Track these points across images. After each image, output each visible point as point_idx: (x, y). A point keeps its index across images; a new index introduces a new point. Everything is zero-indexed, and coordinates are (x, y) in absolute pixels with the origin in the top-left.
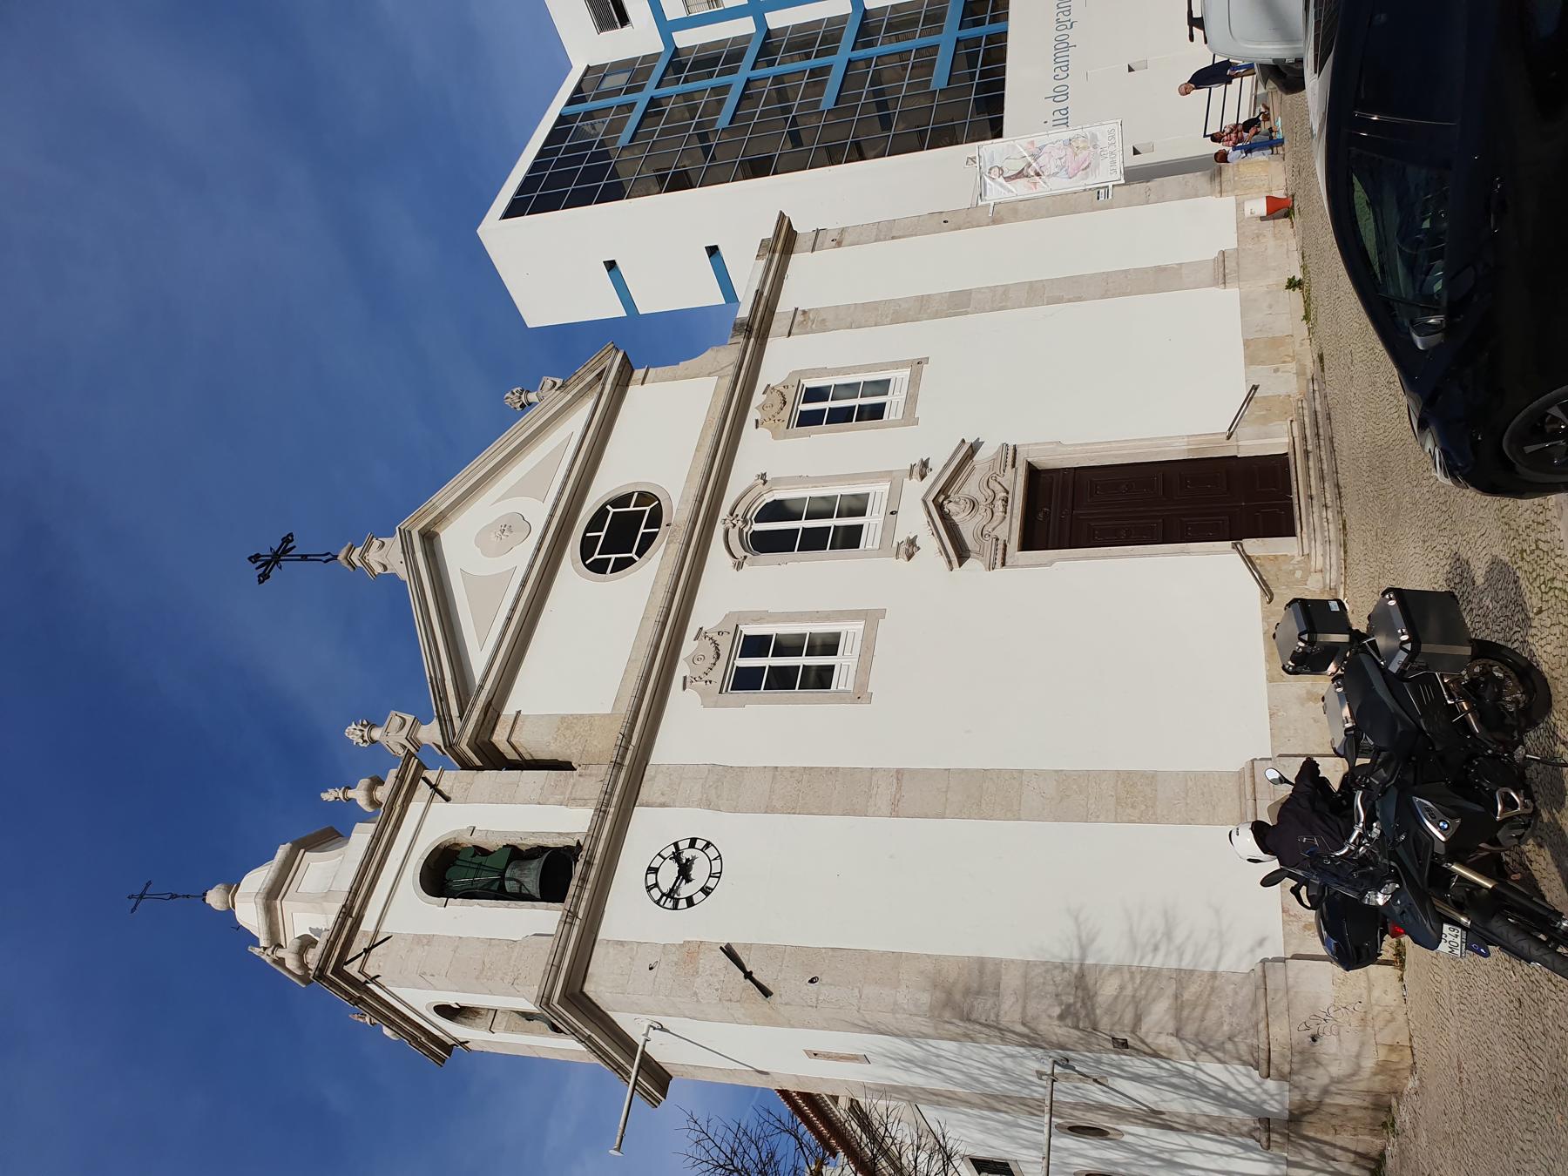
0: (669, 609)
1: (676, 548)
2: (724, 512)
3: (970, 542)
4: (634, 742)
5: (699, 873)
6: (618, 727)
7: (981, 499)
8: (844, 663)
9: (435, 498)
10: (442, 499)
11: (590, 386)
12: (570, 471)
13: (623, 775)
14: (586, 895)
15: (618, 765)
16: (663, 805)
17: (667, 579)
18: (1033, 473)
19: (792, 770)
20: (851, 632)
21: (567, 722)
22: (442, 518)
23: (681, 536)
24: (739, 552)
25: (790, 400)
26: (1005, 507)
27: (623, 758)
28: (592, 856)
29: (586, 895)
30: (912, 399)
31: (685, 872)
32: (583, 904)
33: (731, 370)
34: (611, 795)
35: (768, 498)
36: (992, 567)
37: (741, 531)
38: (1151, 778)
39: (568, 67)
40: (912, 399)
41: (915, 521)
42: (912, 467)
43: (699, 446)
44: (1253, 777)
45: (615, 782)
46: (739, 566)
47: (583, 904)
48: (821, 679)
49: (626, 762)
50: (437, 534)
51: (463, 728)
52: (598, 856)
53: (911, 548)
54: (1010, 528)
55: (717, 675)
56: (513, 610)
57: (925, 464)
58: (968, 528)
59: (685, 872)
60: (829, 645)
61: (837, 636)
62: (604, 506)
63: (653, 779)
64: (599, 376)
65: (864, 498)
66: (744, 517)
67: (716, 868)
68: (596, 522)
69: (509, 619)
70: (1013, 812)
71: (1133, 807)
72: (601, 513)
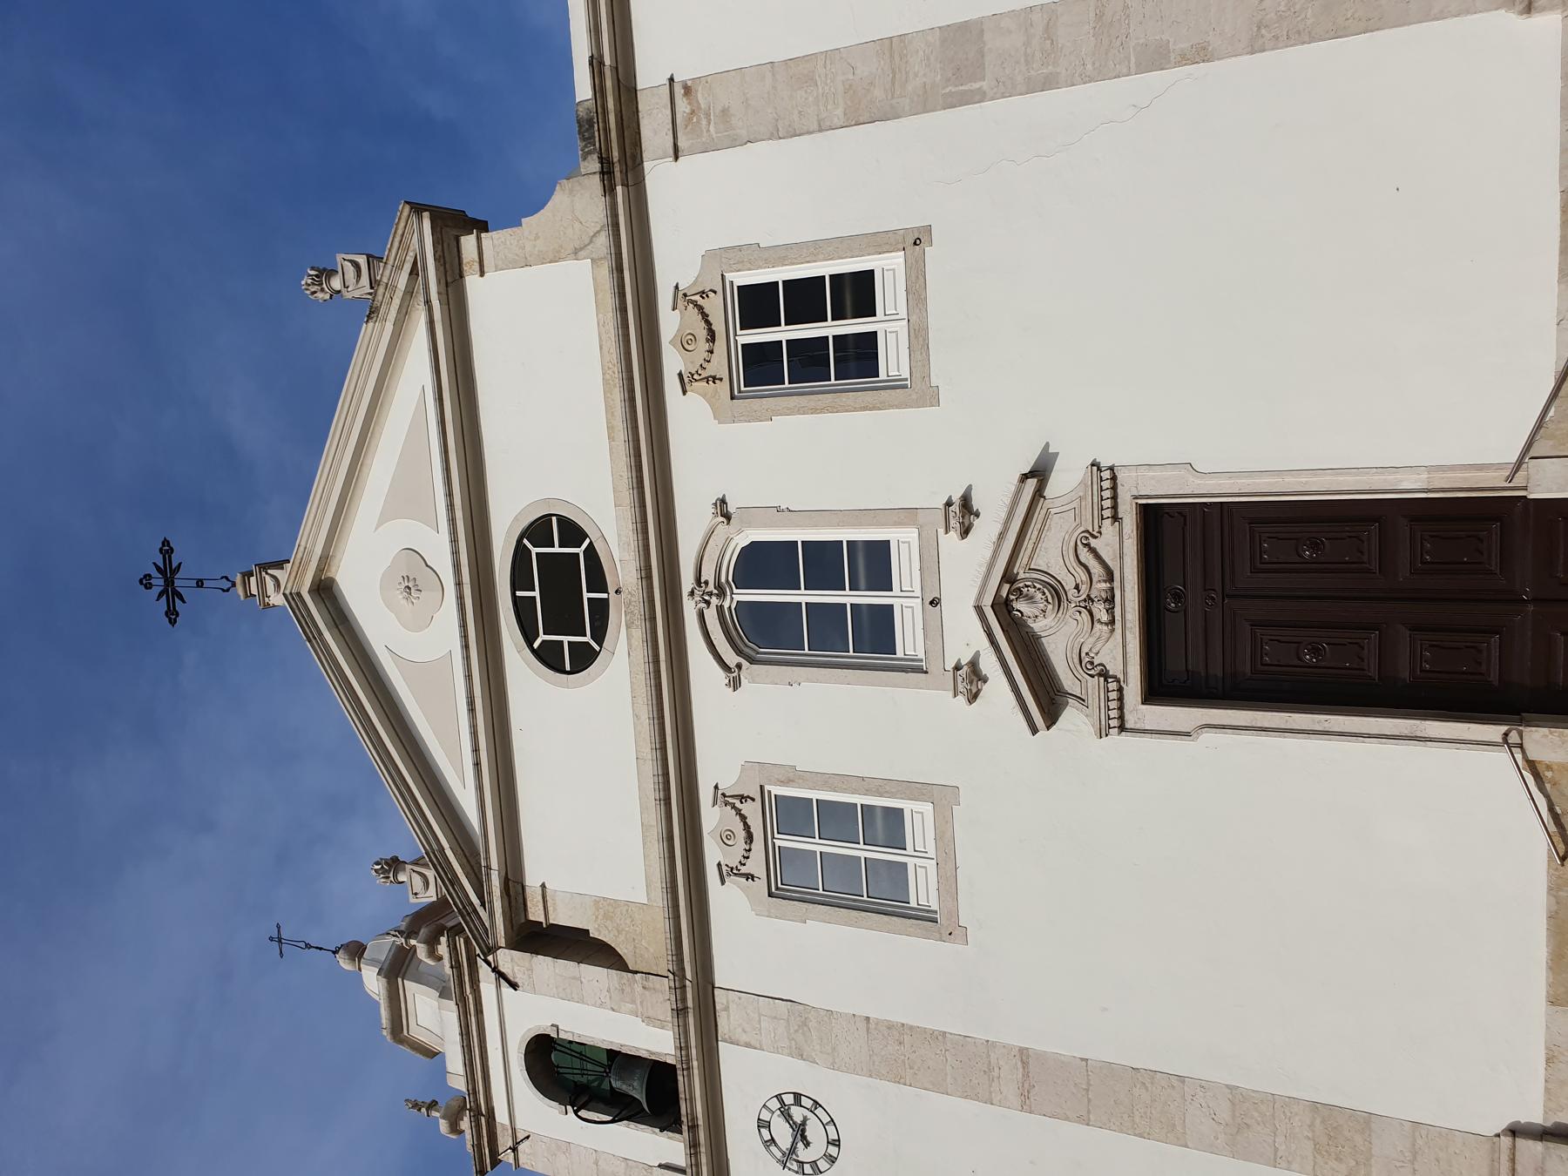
0: (666, 774)
1: (639, 634)
2: (687, 581)
3: (1068, 681)
4: (689, 975)
5: (814, 1131)
6: (660, 900)
7: (1069, 584)
8: (888, 323)
9: (303, 539)
10: (311, 538)
11: (409, 293)
12: (449, 494)
13: (691, 1016)
14: (704, 1160)
15: (680, 1012)
16: (748, 1045)
17: (641, 653)
18: (1154, 518)
19: (890, 1026)
20: (889, 269)
21: (608, 907)
22: (325, 560)
23: (639, 609)
24: (731, 658)
25: (719, 327)
26: (1110, 611)
27: (684, 1000)
28: (694, 1119)
29: (704, 1160)
30: (919, 337)
31: (800, 1131)
32: (694, 1051)
33: (603, 241)
34: (688, 1047)
35: (743, 540)
36: (1103, 732)
37: (720, 609)
38: (1366, 1121)
39: (378, 1003)
40: (919, 337)
41: (966, 636)
42: (949, 504)
43: (610, 428)
44: (1513, 1160)
45: (686, 1032)
46: (735, 684)
47: (694, 1051)
48: (860, 357)
49: (690, 1003)
50: (332, 580)
51: (492, 915)
52: (700, 1115)
53: (971, 678)
54: (1122, 651)
55: (718, 366)
56: (476, 750)
57: (966, 502)
58: (1060, 636)
59: (800, 1131)
60: (857, 293)
61: (870, 274)
62: (533, 651)
63: (727, 1009)
64: (414, 272)
65: (864, 281)
66: (719, 586)
67: (833, 1136)
68: (520, 577)
69: (477, 764)
70: (1174, 1132)
71: (1338, 1159)
72: (521, 556)
